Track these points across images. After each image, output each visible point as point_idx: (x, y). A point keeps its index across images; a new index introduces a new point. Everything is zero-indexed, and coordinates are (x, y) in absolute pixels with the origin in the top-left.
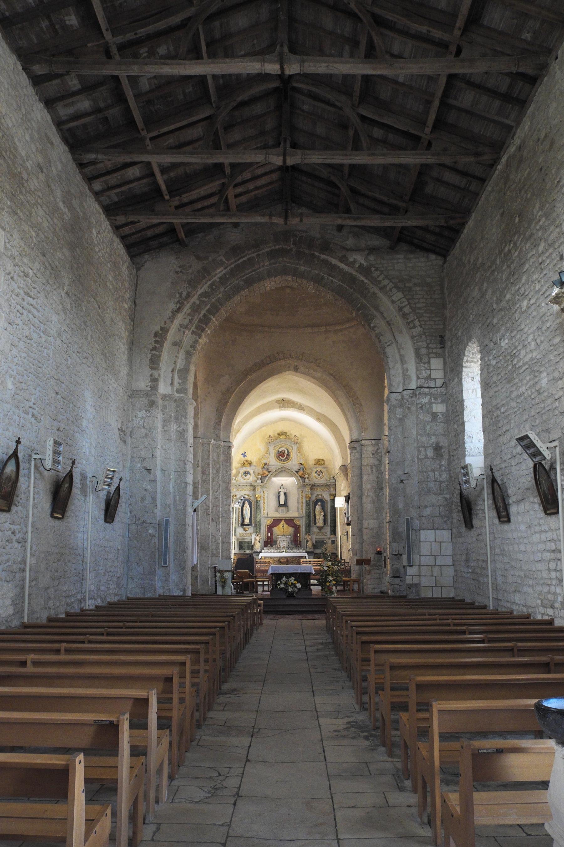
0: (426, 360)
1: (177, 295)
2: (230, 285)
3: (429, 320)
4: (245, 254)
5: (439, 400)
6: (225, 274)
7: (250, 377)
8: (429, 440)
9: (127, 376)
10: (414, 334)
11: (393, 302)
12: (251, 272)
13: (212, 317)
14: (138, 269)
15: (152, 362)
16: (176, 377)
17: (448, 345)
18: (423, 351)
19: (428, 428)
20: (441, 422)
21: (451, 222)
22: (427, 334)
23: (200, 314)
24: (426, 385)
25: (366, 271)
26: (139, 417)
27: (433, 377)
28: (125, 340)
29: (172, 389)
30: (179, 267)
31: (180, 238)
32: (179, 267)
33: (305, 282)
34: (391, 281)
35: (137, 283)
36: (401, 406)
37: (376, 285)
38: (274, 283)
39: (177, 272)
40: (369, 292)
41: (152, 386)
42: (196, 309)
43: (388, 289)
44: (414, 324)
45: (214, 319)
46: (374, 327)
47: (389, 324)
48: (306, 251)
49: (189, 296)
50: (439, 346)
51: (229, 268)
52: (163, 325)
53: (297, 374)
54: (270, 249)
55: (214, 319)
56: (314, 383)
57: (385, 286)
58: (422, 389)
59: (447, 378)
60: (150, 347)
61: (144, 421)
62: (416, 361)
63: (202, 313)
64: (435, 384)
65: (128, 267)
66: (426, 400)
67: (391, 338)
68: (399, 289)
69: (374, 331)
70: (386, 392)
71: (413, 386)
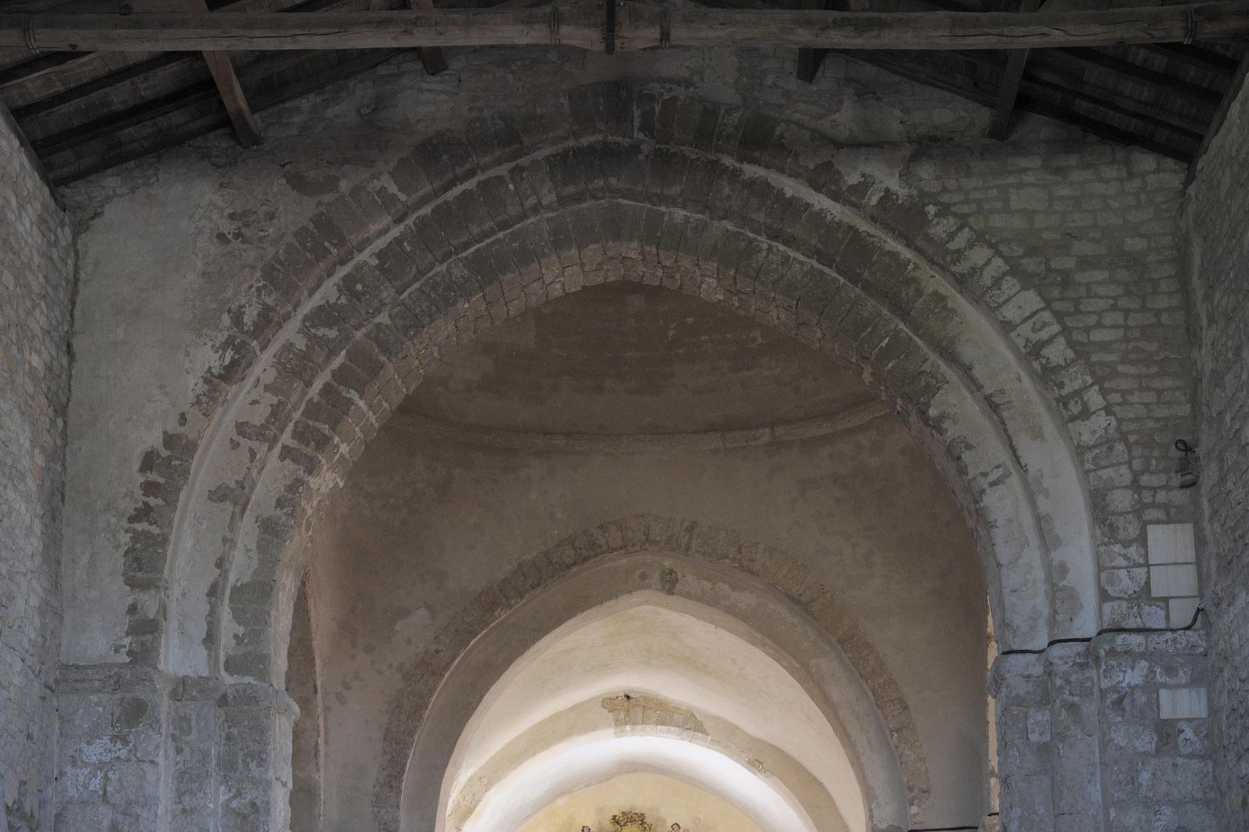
0: (1133, 531)
1: (226, 320)
2: (416, 279)
3: (1141, 389)
4: (467, 166)
5: (1183, 677)
6: (398, 241)
7: (503, 615)
8: (1149, 822)
9: (42, 613)
10: (1087, 438)
11: (1007, 327)
12: (493, 232)
13: (354, 395)
14: (80, 228)
15: (137, 560)
16: (226, 613)
17: (1209, 474)
18: (1122, 500)
19: (1145, 777)
20: (1191, 756)
21: (1209, 30)
22: (1132, 438)
23: (308, 384)
24: (1132, 623)
25: (904, 219)
26: (86, 765)
27: (1157, 592)
28: (31, 484)
29: (213, 660)
30: (232, 217)
31: (230, 109)
32: (232, 217)
33: (686, 263)
34: (998, 253)
35: (77, 279)
36: (1045, 701)
37: (944, 268)
38: (576, 269)
39: (221, 237)
40: (919, 292)
41: (136, 648)
42: (295, 368)
43: (987, 279)
44: (1085, 405)
45: (361, 403)
46: (943, 417)
47: (992, 406)
48: (691, 153)
49: (267, 322)
50: (1176, 480)
51: (410, 221)
52: (173, 427)
53: (673, 599)
54: (560, 147)
55: (361, 403)
56: (732, 631)
57: (975, 271)
58: (1120, 639)
59: (1208, 593)
60: (129, 507)
61: (106, 778)
62: (1093, 536)
63: (318, 384)
64: (1167, 617)
65: (42, 221)
66: (1133, 676)
67: (1004, 457)
68: (1028, 281)
69: (941, 431)
70: (993, 652)
71: (1087, 625)
